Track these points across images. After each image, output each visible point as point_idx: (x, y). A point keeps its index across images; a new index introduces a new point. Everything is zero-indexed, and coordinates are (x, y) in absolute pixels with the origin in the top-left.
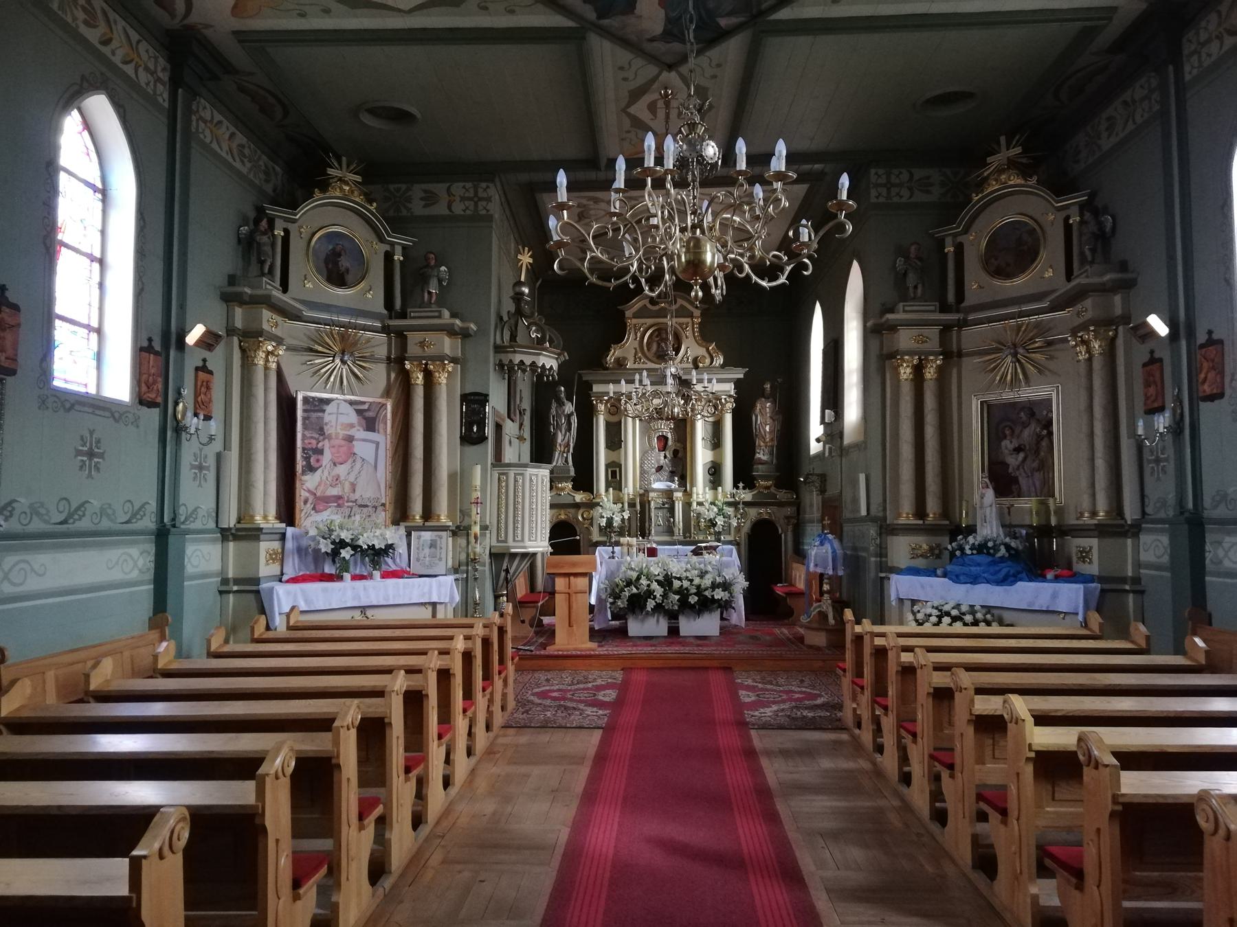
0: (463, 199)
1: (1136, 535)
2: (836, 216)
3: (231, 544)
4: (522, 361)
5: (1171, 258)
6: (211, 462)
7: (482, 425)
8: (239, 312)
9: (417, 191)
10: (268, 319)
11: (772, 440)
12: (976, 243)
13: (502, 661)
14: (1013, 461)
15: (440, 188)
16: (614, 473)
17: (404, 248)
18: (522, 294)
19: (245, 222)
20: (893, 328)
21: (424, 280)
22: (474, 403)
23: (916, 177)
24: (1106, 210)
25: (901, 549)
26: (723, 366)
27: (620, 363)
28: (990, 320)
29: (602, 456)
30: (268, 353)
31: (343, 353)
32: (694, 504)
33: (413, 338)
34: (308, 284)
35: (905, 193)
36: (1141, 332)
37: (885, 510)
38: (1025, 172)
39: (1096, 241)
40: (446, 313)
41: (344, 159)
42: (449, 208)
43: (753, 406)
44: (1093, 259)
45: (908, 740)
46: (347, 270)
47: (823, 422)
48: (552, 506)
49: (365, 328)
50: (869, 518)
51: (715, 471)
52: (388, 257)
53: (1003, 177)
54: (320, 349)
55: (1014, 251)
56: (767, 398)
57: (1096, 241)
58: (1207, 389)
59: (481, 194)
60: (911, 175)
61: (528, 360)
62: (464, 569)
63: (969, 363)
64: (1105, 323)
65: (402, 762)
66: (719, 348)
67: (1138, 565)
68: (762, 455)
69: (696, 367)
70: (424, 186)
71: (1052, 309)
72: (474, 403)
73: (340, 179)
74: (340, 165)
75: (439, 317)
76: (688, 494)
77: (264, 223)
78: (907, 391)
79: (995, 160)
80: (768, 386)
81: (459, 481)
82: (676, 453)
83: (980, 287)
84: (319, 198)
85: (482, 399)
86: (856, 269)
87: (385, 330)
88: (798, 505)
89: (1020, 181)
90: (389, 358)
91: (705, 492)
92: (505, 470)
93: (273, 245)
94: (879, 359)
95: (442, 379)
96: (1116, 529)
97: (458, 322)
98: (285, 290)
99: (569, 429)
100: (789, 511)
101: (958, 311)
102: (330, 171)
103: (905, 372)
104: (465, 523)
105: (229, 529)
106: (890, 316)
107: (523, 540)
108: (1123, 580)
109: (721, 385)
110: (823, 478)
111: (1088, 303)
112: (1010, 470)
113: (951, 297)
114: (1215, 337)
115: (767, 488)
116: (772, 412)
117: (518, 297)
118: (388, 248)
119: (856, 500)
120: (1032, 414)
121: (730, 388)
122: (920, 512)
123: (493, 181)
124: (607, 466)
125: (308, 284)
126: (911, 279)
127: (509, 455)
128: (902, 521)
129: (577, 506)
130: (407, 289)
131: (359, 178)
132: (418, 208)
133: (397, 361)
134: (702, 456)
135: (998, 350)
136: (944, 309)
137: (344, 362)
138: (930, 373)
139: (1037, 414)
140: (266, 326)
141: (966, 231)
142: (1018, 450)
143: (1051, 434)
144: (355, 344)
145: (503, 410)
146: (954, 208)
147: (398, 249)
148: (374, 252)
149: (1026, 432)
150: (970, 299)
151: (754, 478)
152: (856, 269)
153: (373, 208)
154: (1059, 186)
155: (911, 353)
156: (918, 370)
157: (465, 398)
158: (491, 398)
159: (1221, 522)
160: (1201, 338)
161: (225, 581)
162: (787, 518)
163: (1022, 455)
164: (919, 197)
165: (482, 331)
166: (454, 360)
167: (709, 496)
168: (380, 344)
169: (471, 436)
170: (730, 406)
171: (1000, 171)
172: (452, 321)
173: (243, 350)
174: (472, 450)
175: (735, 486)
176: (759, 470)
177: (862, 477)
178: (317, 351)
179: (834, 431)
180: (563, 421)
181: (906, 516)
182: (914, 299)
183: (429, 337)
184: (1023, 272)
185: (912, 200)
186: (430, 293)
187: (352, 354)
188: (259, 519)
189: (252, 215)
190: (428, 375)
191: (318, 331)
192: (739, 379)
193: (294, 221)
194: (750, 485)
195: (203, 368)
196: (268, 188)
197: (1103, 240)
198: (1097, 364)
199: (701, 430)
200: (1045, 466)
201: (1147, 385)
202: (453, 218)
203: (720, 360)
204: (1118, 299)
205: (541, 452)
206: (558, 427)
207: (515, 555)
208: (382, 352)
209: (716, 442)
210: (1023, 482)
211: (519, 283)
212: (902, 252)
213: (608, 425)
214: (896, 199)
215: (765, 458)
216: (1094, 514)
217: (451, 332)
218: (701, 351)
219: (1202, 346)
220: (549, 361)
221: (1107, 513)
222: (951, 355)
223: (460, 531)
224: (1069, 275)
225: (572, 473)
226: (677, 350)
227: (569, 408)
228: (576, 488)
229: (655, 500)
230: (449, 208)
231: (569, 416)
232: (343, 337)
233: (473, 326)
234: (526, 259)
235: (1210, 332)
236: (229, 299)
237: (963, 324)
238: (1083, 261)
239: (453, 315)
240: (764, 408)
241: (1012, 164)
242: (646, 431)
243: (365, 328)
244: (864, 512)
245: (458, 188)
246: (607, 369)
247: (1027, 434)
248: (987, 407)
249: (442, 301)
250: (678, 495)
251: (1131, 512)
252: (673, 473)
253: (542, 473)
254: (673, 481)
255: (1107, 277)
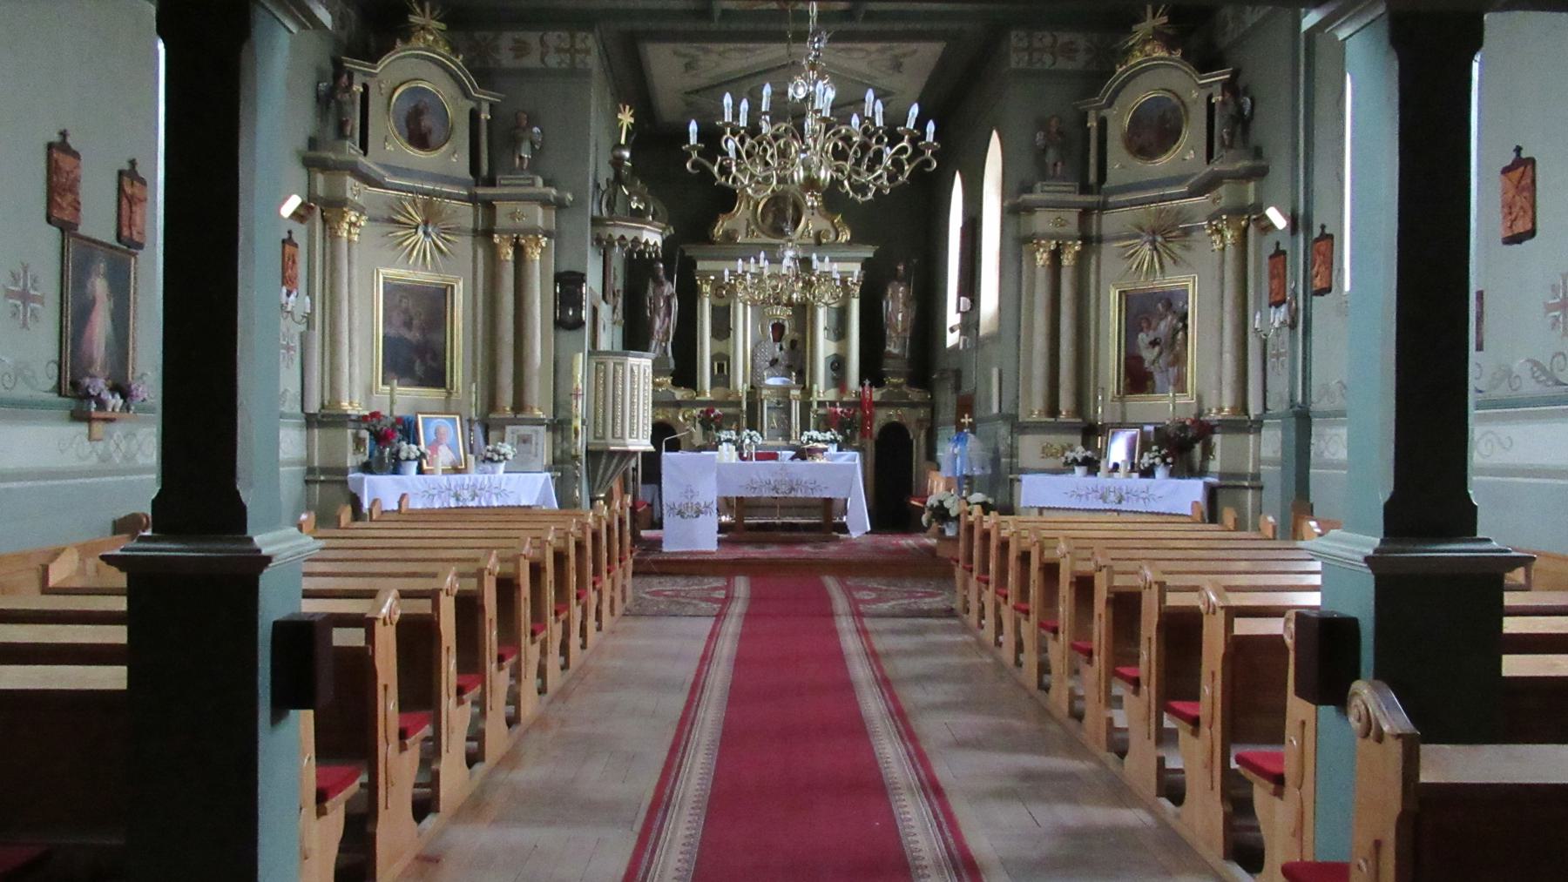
0: (558, 50)
1: (1258, 431)
2: (923, 153)
3: (316, 431)
4: (623, 237)
5: (1295, 148)
6: (296, 343)
7: (578, 306)
8: (320, 179)
9: (506, 39)
10: (353, 188)
11: (904, 330)
12: (1120, 120)
13: (597, 572)
14: (1149, 355)
15: (532, 38)
16: (721, 367)
17: (492, 105)
18: (621, 159)
19: (321, 76)
20: (1030, 209)
21: (514, 143)
22: (569, 284)
23: (1059, 42)
24: (1246, 92)
25: (1030, 448)
26: (849, 243)
27: (729, 237)
28: (1132, 203)
29: (706, 345)
30: (351, 224)
31: (426, 223)
32: (815, 405)
33: (502, 208)
34: (389, 145)
35: (1048, 59)
36: (1264, 224)
37: (1017, 406)
38: (1170, 45)
39: (1236, 125)
40: (540, 181)
41: (427, 5)
42: (542, 60)
43: (884, 291)
44: (1231, 141)
45: (1001, 600)
46: (430, 131)
47: (958, 311)
48: (655, 404)
49: (449, 196)
50: (1002, 416)
51: (838, 365)
52: (474, 116)
53: (1148, 48)
54: (402, 219)
55: (1155, 132)
56: (900, 281)
57: (1236, 125)
58: (1318, 283)
59: (579, 45)
60: (1055, 40)
61: (629, 235)
62: (560, 464)
63: (1109, 250)
64: (1237, 211)
65: (529, 627)
66: (846, 220)
67: (1258, 461)
68: (892, 348)
69: (819, 243)
70: (517, 35)
71: (1190, 194)
72: (569, 284)
73: (423, 28)
74: (423, 10)
75: (533, 185)
76: (807, 392)
77: (345, 79)
78: (1042, 277)
79: (1143, 28)
80: (901, 268)
81: (560, 370)
82: (793, 344)
83: (1122, 167)
84: (400, 50)
85: (580, 278)
86: (995, 135)
87: (472, 199)
88: (932, 407)
89: (1164, 54)
90: (475, 231)
91: (827, 388)
92: (603, 358)
93: (353, 103)
94: (1017, 244)
95: (535, 255)
96: (1241, 424)
97: (554, 191)
98: (365, 154)
99: (669, 314)
100: (922, 413)
101: (1099, 193)
102: (413, 19)
103: (1042, 258)
104: (561, 416)
105: (314, 415)
106: (1026, 197)
107: (622, 437)
108: (1243, 477)
109: (843, 268)
110: (958, 374)
111: (1222, 190)
112: (1146, 364)
113: (1093, 178)
114: (1327, 231)
115: (896, 386)
116: (906, 296)
117: (617, 162)
118: (472, 104)
119: (988, 399)
120: (1169, 305)
121: (856, 268)
122: (1053, 409)
123: (592, 31)
124: (713, 358)
125: (389, 145)
126: (1051, 156)
127: (604, 344)
128: (1035, 417)
129: (678, 405)
130: (495, 149)
131: (443, 26)
132: (506, 59)
133: (484, 234)
134: (825, 347)
135: (1138, 236)
136: (1085, 189)
137: (425, 233)
138: (1067, 260)
139: (1172, 303)
140: (349, 195)
141: (1110, 104)
142: (1154, 343)
143: (1185, 326)
144: (439, 213)
145: (599, 292)
146: (1097, 78)
147: (485, 107)
148: (457, 110)
149: (1163, 325)
150: (1113, 178)
151: (883, 375)
152: (995, 135)
153: (458, 61)
154: (1205, 62)
155: (1050, 237)
156: (1056, 256)
157: (559, 277)
158: (588, 278)
159: (1325, 415)
160: (1317, 233)
161: (311, 470)
162: (919, 421)
163: (1157, 349)
164: (1063, 64)
165: (579, 202)
166: (547, 234)
167: (831, 395)
168: (466, 215)
169: (567, 319)
170: (858, 289)
171: (1145, 42)
172: (547, 189)
173: (325, 220)
174: (565, 335)
175: (861, 384)
176: (888, 366)
177: (995, 372)
178: (399, 222)
179: (970, 321)
180: (661, 304)
181: (1034, 408)
182: (1054, 177)
183: (521, 207)
184: (1166, 151)
185: (1057, 66)
186: (521, 158)
187: (435, 225)
188: (345, 404)
189: (328, 66)
190: (519, 250)
191: (400, 199)
192: (868, 259)
193: (372, 75)
194: (878, 382)
195: (288, 241)
196: (344, 35)
197: (1242, 123)
198: (1230, 253)
199: (822, 318)
200: (1179, 360)
201: (1272, 277)
202: (547, 72)
203: (845, 236)
204: (1251, 186)
205: (635, 338)
206: (655, 311)
207: (615, 452)
208: (468, 223)
209: (840, 332)
210: (1157, 377)
211: (618, 146)
212: (1042, 124)
213: (715, 310)
214: (1038, 66)
215: (896, 351)
216: (1221, 410)
217: (545, 202)
218: (824, 225)
219: (1317, 240)
220: (652, 237)
221: (1233, 409)
222: (1090, 241)
223: (559, 426)
224: (1210, 155)
225: (672, 365)
226: (796, 223)
227: (669, 288)
228: (676, 383)
229: (768, 399)
230: (542, 60)
231: (668, 300)
232: (427, 206)
233: (569, 197)
234: (626, 118)
235: (1323, 227)
236: (312, 163)
237: (1104, 207)
238: (1223, 144)
239: (547, 183)
240: (895, 292)
241: (1158, 34)
242: (760, 317)
243: (449, 196)
244: (995, 410)
245: (552, 37)
246: (712, 242)
247: (1163, 327)
248: (1127, 298)
249: (534, 168)
250: (795, 393)
251: (1254, 409)
252: (790, 368)
253: (641, 364)
254: (789, 376)
255: (1239, 165)
